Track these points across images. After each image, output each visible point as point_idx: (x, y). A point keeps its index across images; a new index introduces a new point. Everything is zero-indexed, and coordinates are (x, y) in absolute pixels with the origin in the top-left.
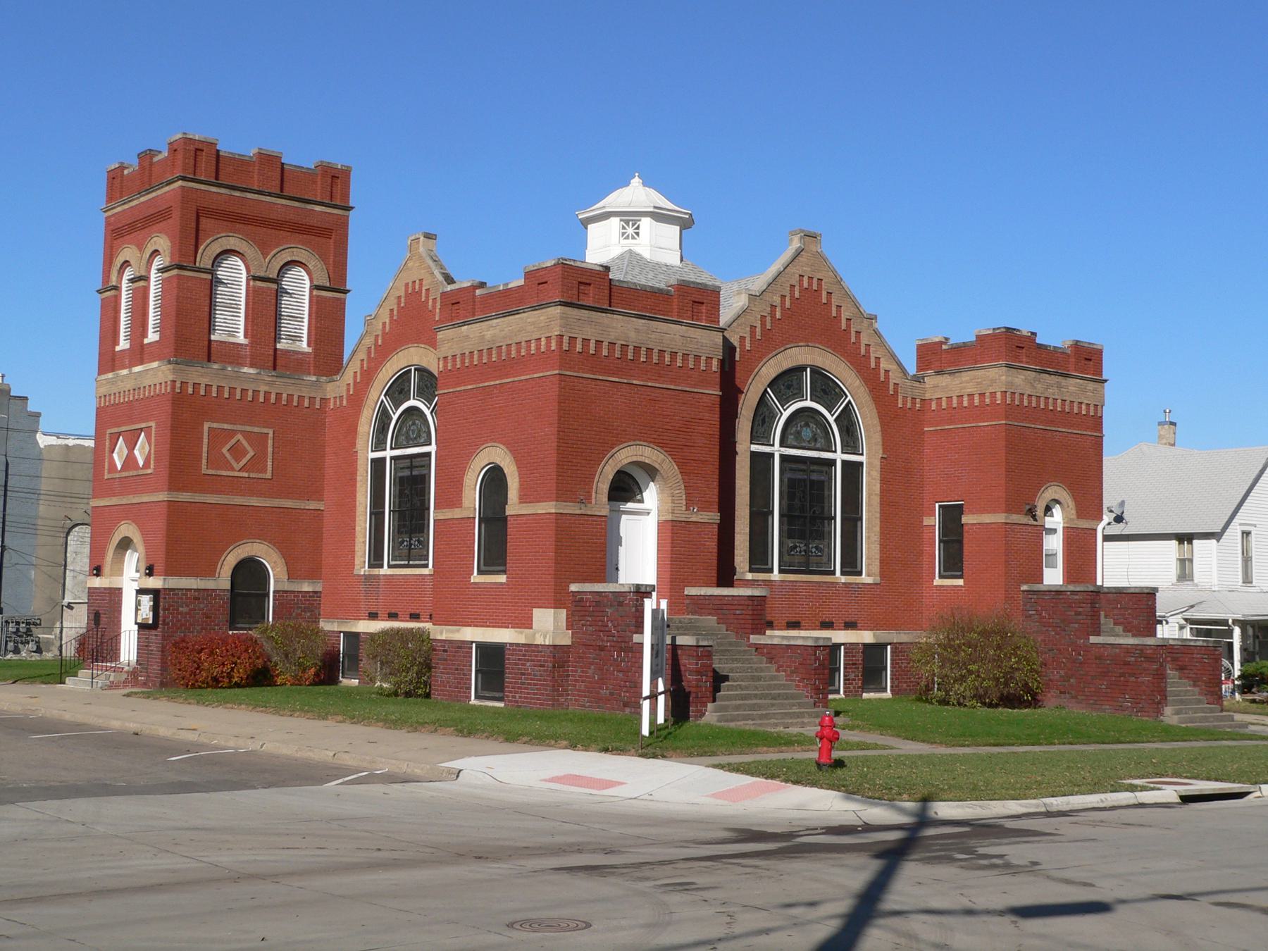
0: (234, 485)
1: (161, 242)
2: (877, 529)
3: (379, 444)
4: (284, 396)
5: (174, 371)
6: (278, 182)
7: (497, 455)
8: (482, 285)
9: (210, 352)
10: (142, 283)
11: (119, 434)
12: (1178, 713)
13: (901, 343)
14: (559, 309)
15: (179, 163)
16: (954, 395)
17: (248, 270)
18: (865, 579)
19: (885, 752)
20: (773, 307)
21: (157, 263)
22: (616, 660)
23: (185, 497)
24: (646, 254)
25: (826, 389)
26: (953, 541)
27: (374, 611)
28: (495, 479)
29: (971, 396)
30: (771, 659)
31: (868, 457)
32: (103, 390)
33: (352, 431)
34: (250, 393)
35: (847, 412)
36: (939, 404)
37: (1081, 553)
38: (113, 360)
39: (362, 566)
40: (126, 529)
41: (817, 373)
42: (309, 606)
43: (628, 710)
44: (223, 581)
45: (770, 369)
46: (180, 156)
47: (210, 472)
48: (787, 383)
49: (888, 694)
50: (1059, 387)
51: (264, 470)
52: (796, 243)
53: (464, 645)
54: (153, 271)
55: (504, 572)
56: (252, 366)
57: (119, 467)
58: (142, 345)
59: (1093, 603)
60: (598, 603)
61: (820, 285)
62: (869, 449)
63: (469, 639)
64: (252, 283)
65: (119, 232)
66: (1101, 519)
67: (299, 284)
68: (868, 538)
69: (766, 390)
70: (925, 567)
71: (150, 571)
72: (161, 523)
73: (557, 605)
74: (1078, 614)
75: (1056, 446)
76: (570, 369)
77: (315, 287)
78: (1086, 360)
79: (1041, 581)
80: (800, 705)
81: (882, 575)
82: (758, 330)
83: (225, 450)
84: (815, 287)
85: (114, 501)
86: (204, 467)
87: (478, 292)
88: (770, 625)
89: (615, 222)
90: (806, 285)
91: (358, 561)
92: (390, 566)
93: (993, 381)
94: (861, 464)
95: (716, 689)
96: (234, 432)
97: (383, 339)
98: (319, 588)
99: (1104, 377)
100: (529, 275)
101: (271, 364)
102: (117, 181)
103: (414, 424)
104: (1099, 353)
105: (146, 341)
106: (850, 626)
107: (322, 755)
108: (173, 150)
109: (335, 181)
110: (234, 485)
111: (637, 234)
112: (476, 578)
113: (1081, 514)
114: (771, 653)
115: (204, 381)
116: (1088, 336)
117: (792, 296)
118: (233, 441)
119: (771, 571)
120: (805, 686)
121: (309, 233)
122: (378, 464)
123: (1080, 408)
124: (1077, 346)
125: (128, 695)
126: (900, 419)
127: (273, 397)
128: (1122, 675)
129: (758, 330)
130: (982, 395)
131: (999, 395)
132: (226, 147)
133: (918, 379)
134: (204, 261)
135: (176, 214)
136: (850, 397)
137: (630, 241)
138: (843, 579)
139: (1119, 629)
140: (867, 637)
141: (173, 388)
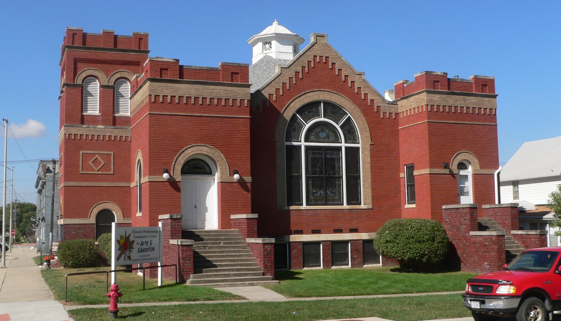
0: (95, 177)
6: (113, 43)
9: (83, 120)
17: (100, 83)
18: (362, 206)
19: (236, 301)
24: (274, 56)
25: (334, 110)
31: (362, 144)
36: (403, 115)
37: (485, 188)
41: (327, 104)
44: (92, 220)
45: (297, 104)
48: (309, 109)
49: (381, 264)
50: (465, 100)
51: (110, 170)
56: (102, 125)
62: (362, 140)
66: (498, 168)
68: (364, 185)
77: (101, 86)
78: (485, 87)
89: (260, 44)
90: (318, 60)
93: (422, 100)
94: (358, 148)
99: (496, 94)
101: (112, 123)
104: (493, 81)
110: (95, 177)
111: (271, 47)
115: (79, 133)
116: (485, 73)
118: (94, 158)
119: (302, 205)
126: (384, 126)
127: (113, 138)
128: (484, 252)
129: (288, 85)
134: (79, 81)
136: (349, 115)
137: (268, 51)
138: (348, 207)
140: (365, 236)
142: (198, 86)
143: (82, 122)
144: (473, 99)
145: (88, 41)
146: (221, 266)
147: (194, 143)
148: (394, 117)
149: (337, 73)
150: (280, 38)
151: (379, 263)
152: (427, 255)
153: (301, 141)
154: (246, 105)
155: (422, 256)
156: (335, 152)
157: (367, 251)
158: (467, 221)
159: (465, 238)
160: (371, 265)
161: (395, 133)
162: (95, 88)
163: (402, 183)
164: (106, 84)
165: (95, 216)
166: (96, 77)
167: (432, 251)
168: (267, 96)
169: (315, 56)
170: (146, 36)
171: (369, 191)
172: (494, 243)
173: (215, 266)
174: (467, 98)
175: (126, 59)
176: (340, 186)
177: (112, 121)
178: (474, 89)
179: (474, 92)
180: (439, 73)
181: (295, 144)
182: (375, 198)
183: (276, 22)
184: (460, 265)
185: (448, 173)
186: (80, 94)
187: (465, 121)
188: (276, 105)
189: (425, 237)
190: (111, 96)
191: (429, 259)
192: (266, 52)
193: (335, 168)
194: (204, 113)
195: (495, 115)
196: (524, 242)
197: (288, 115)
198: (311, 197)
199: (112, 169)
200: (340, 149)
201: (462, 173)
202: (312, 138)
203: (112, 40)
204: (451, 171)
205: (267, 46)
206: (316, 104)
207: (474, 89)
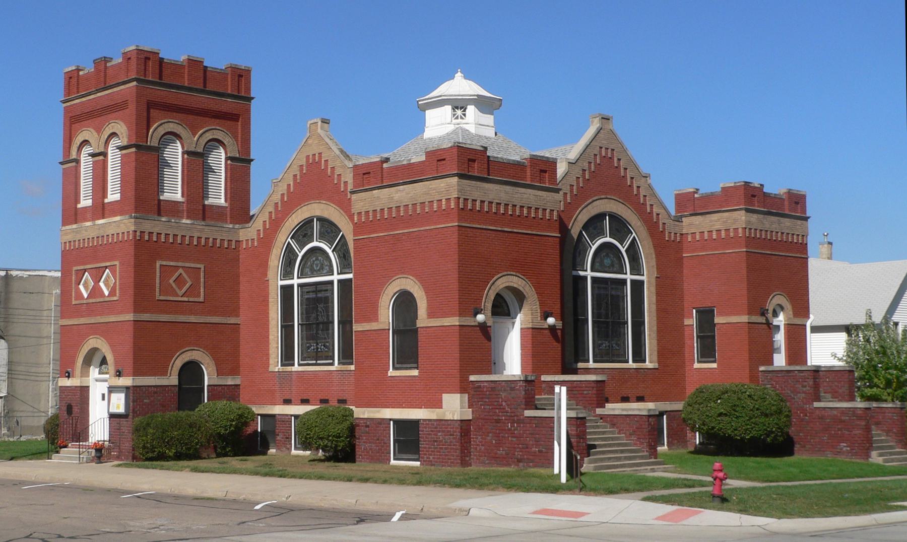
1: (120, 127)
2: (655, 328)
5: (136, 224)
6: (202, 80)
8: (387, 160)
9: (162, 208)
10: (101, 158)
12: (881, 455)
14: (456, 179)
18: (648, 364)
21: (115, 142)
22: (509, 430)
23: (146, 317)
24: (472, 129)
25: (620, 228)
26: (708, 336)
27: (288, 398)
28: (405, 302)
29: (719, 231)
30: (613, 425)
33: (264, 266)
34: (187, 238)
35: (633, 246)
39: (276, 366)
41: (614, 218)
42: (232, 393)
43: (521, 464)
44: (173, 380)
45: (583, 216)
46: (134, 61)
47: (162, 298)
48: (594, 225)
49: (666, 447)
51: (199, 296)
53: (385, 422)
54: (110, 149)
55: (417, 368)
56: (188, 218)
57: (86, 296)
58: (103, 204)
59: (815, 378)
60: (493, 389)
61: (613, 154)
63: (388, 417)
64: (229, 162)
65: (75, 120)
66: (808, 317)
67: (219, 159)
68: (650, 335)
69: (581, 232)
73: (462, 391)
74: (803, 386)
75: (776, 265)
76: (466, 221)
77: (227, 159)
79: (772, 364)
80: (642, 457)
81: (659, 362)
83: (171, 281)
85: (82, 321)
87: (385, 165)
88: (607, 401)
89: (448, 108)
91: (271, 361)
92: (299, 365)
93: (735, 220)
94: (642, 282)
96: (177, 267)
97: (288, 197)
98: (238, 382)
99: (252, 157)
101: (201, 216)
102: (74, 81)
103: (317, 259)
104: (803, 197)
106: (640, 399)
108: (127, 57)
109: (241, 76)
111: (464, 115)
112: (391, 372)
114: (613, 420)
115: (156, 230)
117: (595, 162)
118: (177, 274)
119: (588, 361)
120: (642, 443)
122: (287, 291)
123: (793, 238)
124: (790, 193)
125: (119, 465)
126: (669, 250)
127: (203, 241)
130: (727, 230)
131: (740, 230)
133: (678, 219)
135: (132, 108)
137: (459, 120)
138: (635, 365)
139: (829, 396)
141: (135, 236)
143: (159, 214)
144: (787, 222)
145: (166, 72)
146: (601, 446)
158: (808, 388)
159: (804, 411)
162: (175, 154)
164: (193, 149)
166: (178, 136)
169: (601, 148)
171: (655, 342)
172: (860, 418)
179: (787, 212)
181: (582, 273)
182: (662, 354)
183: (459, 74)
185: (764, 321)
189: (773, 408)
191: (775, 438)
200: (625, 281)
204: (767, 319)
205: (459, 112)
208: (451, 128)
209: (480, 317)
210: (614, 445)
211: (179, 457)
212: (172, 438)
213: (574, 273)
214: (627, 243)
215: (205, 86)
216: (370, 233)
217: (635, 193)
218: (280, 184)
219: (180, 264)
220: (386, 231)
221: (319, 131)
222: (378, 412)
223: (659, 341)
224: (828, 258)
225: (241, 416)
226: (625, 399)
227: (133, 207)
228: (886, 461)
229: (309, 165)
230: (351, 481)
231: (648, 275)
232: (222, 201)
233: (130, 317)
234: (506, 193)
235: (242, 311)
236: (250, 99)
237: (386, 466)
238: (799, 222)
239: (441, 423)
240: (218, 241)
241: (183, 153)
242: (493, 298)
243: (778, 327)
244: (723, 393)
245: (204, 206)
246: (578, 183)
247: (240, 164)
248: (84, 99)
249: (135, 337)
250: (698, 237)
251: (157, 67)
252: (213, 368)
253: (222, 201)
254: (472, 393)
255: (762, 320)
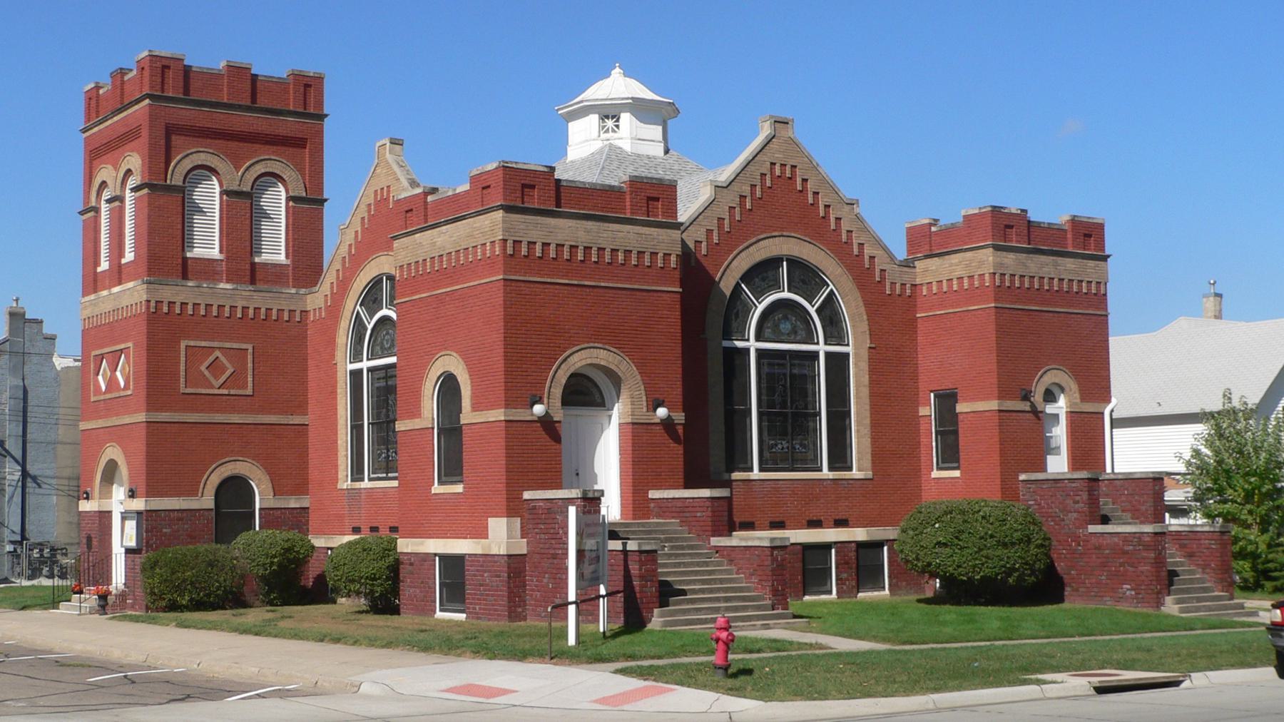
0: (212, 402)
1: (134, 161)
2: (868, 421)
3: (357, 357)
4: (263, 310)
6: (248, 94)
7: (452, 363)
8: (434, 191)
9: (186, 269)
10: (117, 204)
11: (102, 357)
12: (1178, 602)
13: (887, 224)
14: (500, 213)
15: (146, 80)
16: (944, 279)
18: (855, 473)
20: (743, 197)
21: (132, 182)
24: (626, 146)
25: (806, 277)
28: (449, 386)
30: (731, 561)
31: (854, 347)
32: (88, 313)
33: (332, 343)
36: (930, 289)
37: (1087, 442)
38: (95, 281)
39: (345, 483)
40: (112, 452)
41: (795, 263)
42: (299, 519)
45: (743, 262)
46: (147, 73)
48: (762, 275)
49: (887, 592)
50: (1056, 265)
51: (245, 386)
52: (765, 131)
53: (428, 558)
54: (128, 191)
56: (228, 281)
58: (120, 266)
62: (855, 338)
64: (291, 203)
65: (97, 153)
66: (1109, 401)
67: (276, 201)
68: (858, 431)
69: (738, 285)
70: (923, 459)
71: (132, 494)
72: (140, 447)
73: (511, 512)
76: (515, 273)
77: (289, 199)
78: (1087, 238)
82: (727, 222)
84: (788, 175)
85: (100, 423)
86: (182, 385)
87: (430, 198)
89: (594, 119)
90: (778, 172)
91: (341, 475)
93: (981, 263)
94: (848, 355)
95: (1171, 583)
99: (1107, 253)
100: (474, 180)
104: (1100, 227)
105: (124, 261)
106: (841, 523)
107: (248, 671)
109: (309, 86)
110: (212, 402)
111: (617, 126)
112: (437, 489)
113: (1085, 397)
114: (730, 554)
116: (1089, 211)
118: (211, 359)
119: (751, 470)
120: (764, 587)
121: (284, 144)
124: (1075, 222)
126: (894, 311)
127: (251, 312)
128: (1122, 565)
129: (727, 222)
130: (971, 277)
131: (987, 277)
132: (196, 60)
135: (145, 132)
136: (831, 286)
137: (610, 134)
138: (831, 475)
140: (859, 534)
141: (148, 307)
142: (590, 223)
143: (185, 276)
144: (1069, 263)
145: (195, 84)
147: (584, 342)
148: (908, 291)
149: (811, 201)
150: (640, 109)
151: (883, 588)
152: (1017, 570)
153: (748, 340)
154: (673, 265)
155: (1009, 572)
156: (807, 363)
157: (863, 565)
159: (1077, 539)
160: (870, 594)
161: (911, 325)
162: (210, 195)
163: (923, 428)
164: (235, 188)
165: (213, 492)
166: (213, 171)
167: (1026, 564)
168: (692, 245)
169: (773, 164)
170: (319, 79)
171: (867, 442)
172: (1147, 547)
173: (683, 592)
174: (1060, 260)
175: (277, 132)
176: (816, 431)
177: (248, 273)
178: (1070, 242)
179: (1070, 249)
180: (1014, 211)
181: (739, 344)
182: (879, 457)
183: (617, 70)
184: (1063, 590)
185: (1028, 408)
186: (180, 209)
187: (1051, 307)
188: (704, 262)
189: (1015, 535)
190: (243, 213)
191: (1020, 579)
192: (607, 136)
193: (807, 396)
194: (600, 279)
195: (1105, 295)
196: (1182, 546)
197: (727, 286)
198: (767, 455)
199: (250, 384)
200: (815, 355)
201: (1050, 409)
202: (767, 333)
203: (247, 86)
204: (1033, 406)
205: (610, 123)
206: (772, 263)
207: (1070, 242)
208: (598, 145)
209: (539, 409)
210: (718, 590)
211: (198, 606)
212: (184, 581)
213: (726, 344)
214: (819, 301)
215: (254, 100)
216: (413, 294)
217: (833, 227)
218: (348, 231)
219: (216, 344)
220: (429, 290)
221: (388, 155)
222: (422, 544)
223: (875, 439)
224: (1216, 317)
225: (288, 550)
226: (815, 524)
227: (145, 268)
228: (1182, 610)
229: (377, 203)
230: (322, 641)
231: (855, 345)
232: (281, 258)
233: (141, 417)
234: (588, 232)
235: (311, 407)
236: (322, 117)
237: (425, 619)
238: (1091, 263)
239: (487, 559)
240: (274, 312)
241: (222, 193)
242: (564, 382)
243: (1056, 416)
244: (946, 513)
245: (253, 265)
246: (732, 216)
247: (308, 207)
248: (102, 127)
249: (148, 445)
250: (935, 289)
251: (181, 78)
252: (267, 485)
253: (281, 258)
254: (527, 516)
255: (1026, 406)
